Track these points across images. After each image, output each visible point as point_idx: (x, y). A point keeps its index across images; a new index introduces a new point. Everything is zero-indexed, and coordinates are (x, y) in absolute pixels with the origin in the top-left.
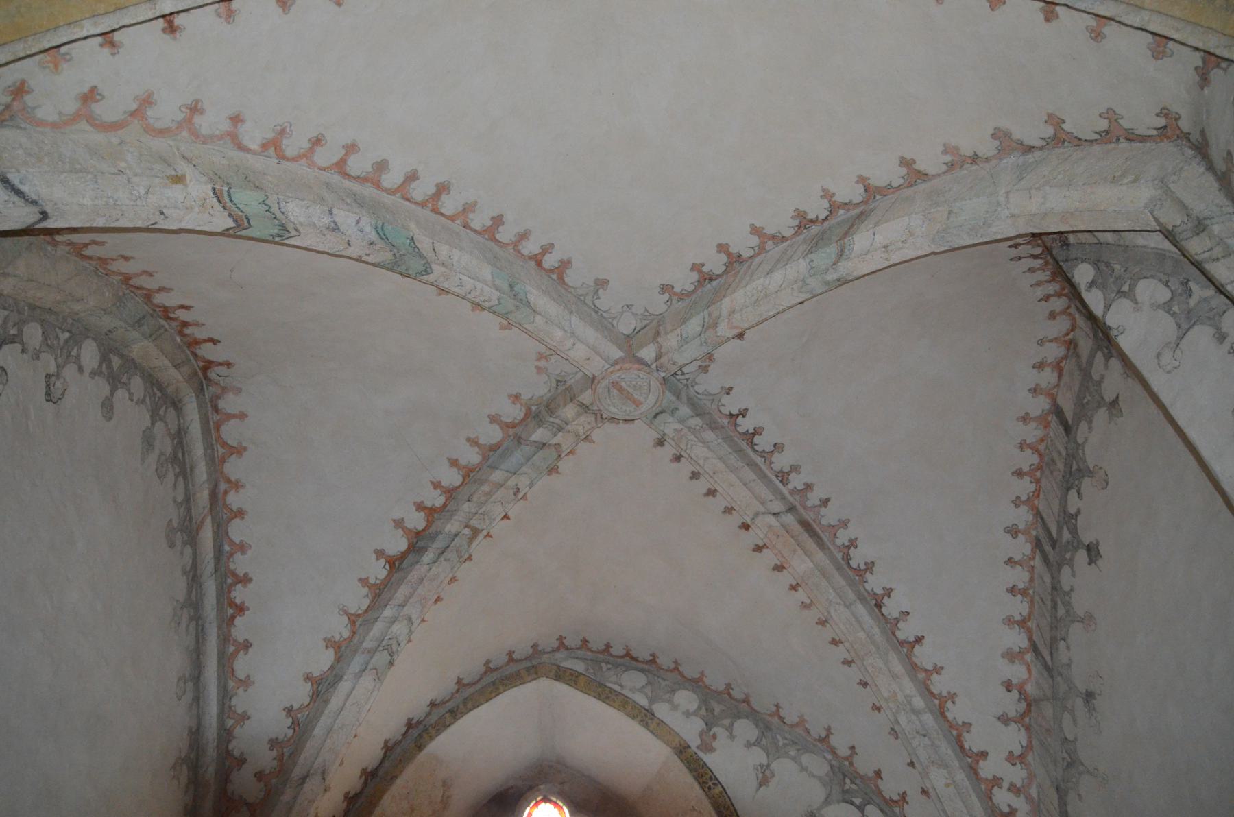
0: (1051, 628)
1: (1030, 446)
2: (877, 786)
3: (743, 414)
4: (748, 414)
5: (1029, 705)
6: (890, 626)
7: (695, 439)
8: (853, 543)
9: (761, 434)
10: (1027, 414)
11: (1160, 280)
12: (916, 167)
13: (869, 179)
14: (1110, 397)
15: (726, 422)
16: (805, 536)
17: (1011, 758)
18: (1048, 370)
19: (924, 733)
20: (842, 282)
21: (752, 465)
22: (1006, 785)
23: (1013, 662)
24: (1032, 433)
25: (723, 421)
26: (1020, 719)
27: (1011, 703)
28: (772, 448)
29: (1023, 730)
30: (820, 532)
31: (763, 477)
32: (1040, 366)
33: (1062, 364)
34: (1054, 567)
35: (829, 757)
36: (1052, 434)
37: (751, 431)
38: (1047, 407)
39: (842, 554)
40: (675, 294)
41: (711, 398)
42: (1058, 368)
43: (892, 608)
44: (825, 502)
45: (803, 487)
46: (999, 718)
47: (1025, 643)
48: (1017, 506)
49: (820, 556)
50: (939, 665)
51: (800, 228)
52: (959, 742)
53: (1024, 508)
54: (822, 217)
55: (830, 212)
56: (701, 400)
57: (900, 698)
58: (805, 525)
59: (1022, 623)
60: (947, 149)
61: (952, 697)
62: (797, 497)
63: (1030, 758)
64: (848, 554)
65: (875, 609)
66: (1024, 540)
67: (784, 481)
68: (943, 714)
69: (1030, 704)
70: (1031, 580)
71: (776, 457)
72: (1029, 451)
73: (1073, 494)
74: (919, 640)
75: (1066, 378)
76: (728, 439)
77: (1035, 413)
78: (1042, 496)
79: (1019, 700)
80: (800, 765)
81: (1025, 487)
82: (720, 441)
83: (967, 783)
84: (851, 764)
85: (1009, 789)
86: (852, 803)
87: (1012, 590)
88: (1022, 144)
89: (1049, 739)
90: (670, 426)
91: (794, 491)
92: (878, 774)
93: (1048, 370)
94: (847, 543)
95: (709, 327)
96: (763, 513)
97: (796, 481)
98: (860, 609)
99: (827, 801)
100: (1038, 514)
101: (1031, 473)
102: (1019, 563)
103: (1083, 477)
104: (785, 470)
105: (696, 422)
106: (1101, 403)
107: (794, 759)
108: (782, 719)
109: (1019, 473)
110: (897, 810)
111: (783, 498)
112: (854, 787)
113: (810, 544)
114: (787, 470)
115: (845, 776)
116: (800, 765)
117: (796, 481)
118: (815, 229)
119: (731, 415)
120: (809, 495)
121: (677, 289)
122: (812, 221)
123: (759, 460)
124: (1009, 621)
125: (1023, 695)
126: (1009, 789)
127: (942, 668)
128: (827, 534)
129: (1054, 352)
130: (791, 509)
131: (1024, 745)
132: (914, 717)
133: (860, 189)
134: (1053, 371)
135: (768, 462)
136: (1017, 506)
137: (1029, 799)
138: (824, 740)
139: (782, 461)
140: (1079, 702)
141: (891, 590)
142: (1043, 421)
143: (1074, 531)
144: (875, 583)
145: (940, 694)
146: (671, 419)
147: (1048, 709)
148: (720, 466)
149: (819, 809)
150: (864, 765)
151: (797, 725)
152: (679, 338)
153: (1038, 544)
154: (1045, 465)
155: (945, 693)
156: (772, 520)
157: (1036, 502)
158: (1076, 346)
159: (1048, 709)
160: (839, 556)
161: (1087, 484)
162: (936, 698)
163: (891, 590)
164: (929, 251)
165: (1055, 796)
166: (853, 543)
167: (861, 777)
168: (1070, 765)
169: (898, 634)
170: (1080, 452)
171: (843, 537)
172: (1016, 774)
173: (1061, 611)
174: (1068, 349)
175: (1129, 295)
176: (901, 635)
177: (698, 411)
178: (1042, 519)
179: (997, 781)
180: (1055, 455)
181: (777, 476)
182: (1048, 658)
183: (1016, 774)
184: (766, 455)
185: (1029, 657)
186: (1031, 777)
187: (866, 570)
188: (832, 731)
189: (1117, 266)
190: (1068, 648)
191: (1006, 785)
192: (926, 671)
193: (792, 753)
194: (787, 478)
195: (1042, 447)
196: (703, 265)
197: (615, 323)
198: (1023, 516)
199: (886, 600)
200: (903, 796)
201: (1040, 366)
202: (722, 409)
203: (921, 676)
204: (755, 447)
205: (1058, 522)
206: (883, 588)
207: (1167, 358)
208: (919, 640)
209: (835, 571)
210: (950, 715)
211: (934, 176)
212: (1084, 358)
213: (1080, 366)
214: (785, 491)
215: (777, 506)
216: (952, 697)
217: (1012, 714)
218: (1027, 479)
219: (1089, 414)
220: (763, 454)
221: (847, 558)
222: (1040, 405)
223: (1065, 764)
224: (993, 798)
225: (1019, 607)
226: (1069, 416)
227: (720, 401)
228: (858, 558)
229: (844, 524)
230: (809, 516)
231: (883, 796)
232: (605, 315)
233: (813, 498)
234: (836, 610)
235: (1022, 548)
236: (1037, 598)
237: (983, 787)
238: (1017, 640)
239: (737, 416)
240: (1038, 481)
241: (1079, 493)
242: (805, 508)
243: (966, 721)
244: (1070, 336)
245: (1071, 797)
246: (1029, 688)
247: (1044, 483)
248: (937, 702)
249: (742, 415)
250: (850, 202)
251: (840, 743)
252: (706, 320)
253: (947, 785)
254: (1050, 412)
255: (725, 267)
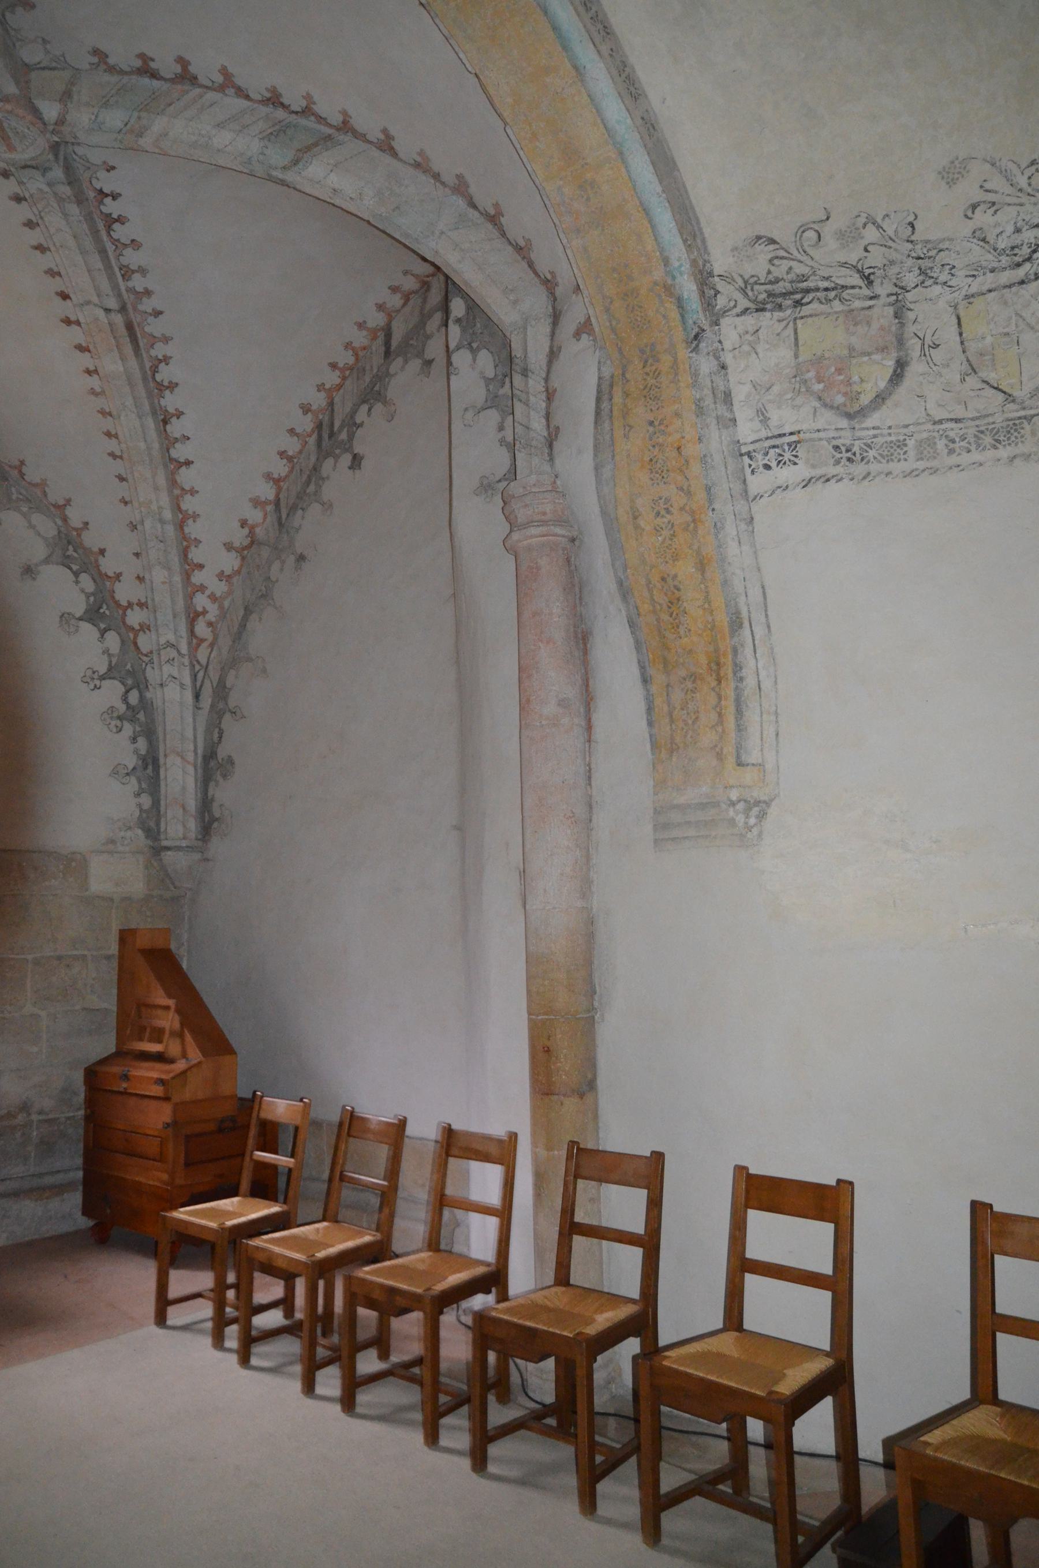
0: (298, 497)
1: (353, 349)
2: (97, 561)
3: (115, 197)
4: (119, 199)
5: (252, 543)
6: (168, 442)
7: (58, 208)
8: (166, 360)
9: (123, 224)
10: (365, 322)
11: (494, 360)
12: (393, 143)
13: (351, 118)
14: (428, 355)
15: (92, 194)
16: (126, 340)
17: (221, 576)
18: (398, 296)
19: (161, 539)
20: (283, 183)
21: (103, 252)
22: (208, 592)
23: (256, 508)
24: (360, 339)
25: (90, 193)
26: (241, 551)
27: (240, 537)
28: (128, 242)
29: (239, 558)
30: (139, 335)
31: (108, 267)
32: (394, 289)
33: (411, 296)
34: (323, 453)
35: (59, 522)
36: (374, 348)
37: (115, 216)
38: (382, 324)
39: (151, 364)
40: (106, 63)
41: (87, 165)
42: (407, 298)
43: (175, 428)
44: (157, 313)
45: (141, 290)
46: (225, 545)
47: (271, 496)
48: (319, 390)
49: (133, 363)
50: (196, 489)
51: (265, 102)
52: (185, 553)
53: (323, 395)
54: (293, 108)
55: (303, 112)
56: (75, 160)
57: (154, 507)
58: (130, 327)
59: (277, 481)
60: (421, 153)
61: (195, 516)
62: (132, 297)
63: (235, 580)
64: (157, 367)
65: (161, 424)
66: (310, 419)
67: (126, 277)
68: (182, 528)
69: (253, 541)
70: (301, 452)
71: (128, 252)
72: (351, 352)
73: (365, 408)
74: (188, 463)
75: (407, 309)
76: (89, 218)
77: (371, 324)
78: (341, 391)
79: (247, 537)
80: (29, 522)
81: (332, 378)
82: (81, 218)
83: (180, 586)
84: (79, 535)
85: (209, 597)
86: (70, 569)
87: (282, 454)
88: (471, 198)
89: (256, 572)
90: (36, 184)
91: (129, 290)
92: (102, 552)
93: (398, 296)
94: (160, 357)
95: (132, 131)
96: (96, 305)
97: (138, 282)
98: (150, 422)
99: (47, 561)
100: (331, 404)
101: (342, 370)
102: (297, 435)
103: (379, 401)
104: (132, 267)
105: (66, 190)
106: (420, 354)
107: (24, 515)
108: (22, 475)
109: (334, 366)
110: (108, 584)
111: (119, 295)
112: (75, 555)
113: (128, 349)
114: (132, 268)
115: (69, 543)
116: (29, 522)
117: (138, 282)
118: (280, 114)
119: (101, 192)
120: (145, 300)
121: (111, 61)
122: (283, 105)
123: (110, 248)
124: (268, 476)
125: (252, 533)
126: (209, 597)
127: (197, 492)
128: (145, 341)
129: (410, 284)
130: (123, 309)
131: (235, 569)
132: (159, 526)
133: (341, 118)
134: (401, 298)
135: (118, 252)
136: (319, 390)
137: (221, 607)
138: (61, 508)
139: (131, 258)
140: (292, 558)
141: (182, 413)
142: (373, 334)
143: (351, 436)
144: (170, 401)
145: (186, 511)
146: (41, 179)
147: (265, 552)
148: (72, 243)
149: (37, 565)
150: (91, 540)
151: (36, 485)
152: (93, 117)
153: (319, 426)
154: (355, 370)
155: (190, 512)
156: (101, 314)
157: (334, 394)
158: (428, 290)
159: (265, 552)
160: (148, 365)
161: (379, 407)
162: (181, 513)
163: (182, 413)
164: (367, 218)
165: (242, 612)
166: (166, 360)
167: (84, 548)
168: (262, 596)
169: (172, 451)
170: (387, 379)
171: (159, 350)
172: (219, 588)
173: (312, 488)
174: (421, 288)
175: (474, 352)
176: (174, 453)
177: (72, 180)
178: (333, 410)
179: (202, 588)
180: (368, 368)
181: (121, 269)
182: (284, 516)
183: (219, 588)
184: (119, 245)
185: (270, 508)
186: (230, 593)
187: (167, 388)
188: (72, 503)
189: (478, 325)
190: (303, 518)
191: (208, 592)
192: (183, 489)
193: (25, 509)
194: (130, 276)
195: (361, 354)
196: (153, 60)
197: (18, 44)
198: (319, 400)
199: (174, 420)
200: (118, 576)
201: (394, 289)
202: (94, 181)
203: (177, 492)
204: (112, 233)
205: (343, 421)
206: (176, 410)
207: (469, 415)
208: (188, 463)
209: (141, 382)
210: (187, 530)
211: (401, 160)
212: (428, 307)
213: (422, 309)
214: (123, 288)
215: (113, 303)
216: (195, 516)
217: (237, 544)
218: (338, 373)
219: (409, 355)
220: (116, 243)
221: (155, 370)
222: (377, 320)
223: (260, 594)
224: (194, 599)
225: (280, 468)
226: (394, 343)
227: (95, 173)
228: (164, 374)
229: (166, 340)
230: (136, 319)
231: (99, 570)
232: (13, 33)
233: (147, 305)
234: (127, 415)
235: (306, 424)
236: (297, 468)
237: (190, 589)
238: (267, 492)
239: (107, 195)
240: (344, 378)
241: (370, 410)
242: (135, 309)
243: (198, 538)
244: (428, 279)
245: (254, 617)
246: (258, 530)
247: (348, 382)
248: (181, 516)
249: (113, 197)
250: (325, 119)
251: (75, 515)
252: (132, 121)
253: (164, 583)
254: (383, 329)
255: (174, 76)
